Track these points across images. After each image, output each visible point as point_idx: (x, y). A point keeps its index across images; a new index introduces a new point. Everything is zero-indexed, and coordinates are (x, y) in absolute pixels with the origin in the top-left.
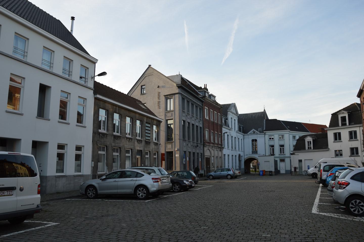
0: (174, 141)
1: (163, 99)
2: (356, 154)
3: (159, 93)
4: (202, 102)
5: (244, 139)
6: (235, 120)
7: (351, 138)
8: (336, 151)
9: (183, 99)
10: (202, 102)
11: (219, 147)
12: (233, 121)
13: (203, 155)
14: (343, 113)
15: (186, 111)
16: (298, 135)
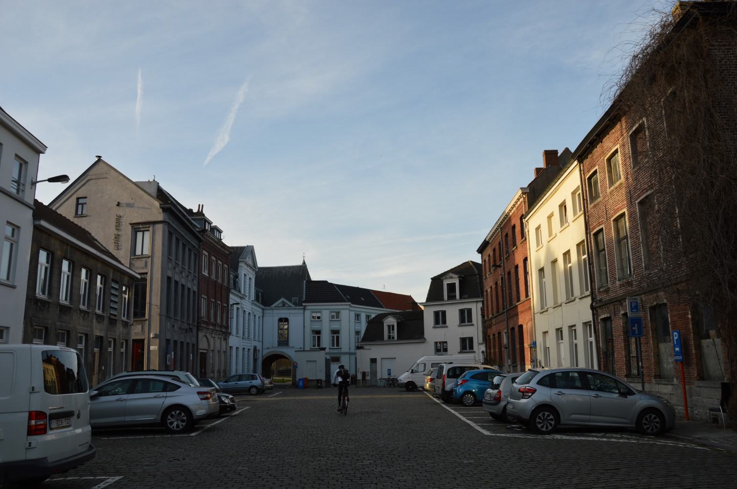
0: (147, 317)
1: (127, 231)
2: (470, 349)
3: (119, 218)
4: (200, 240)
5: (263, 317)
6: (250, 278)
7: (462, 320)
8: (436, 343)
9: (170, 234)
10: (200, 240)
11: (224, 333)
12: (248, 281)
13: (196, 346)
14: (451, 278)
15: (173, 258)
16: (374, 312)
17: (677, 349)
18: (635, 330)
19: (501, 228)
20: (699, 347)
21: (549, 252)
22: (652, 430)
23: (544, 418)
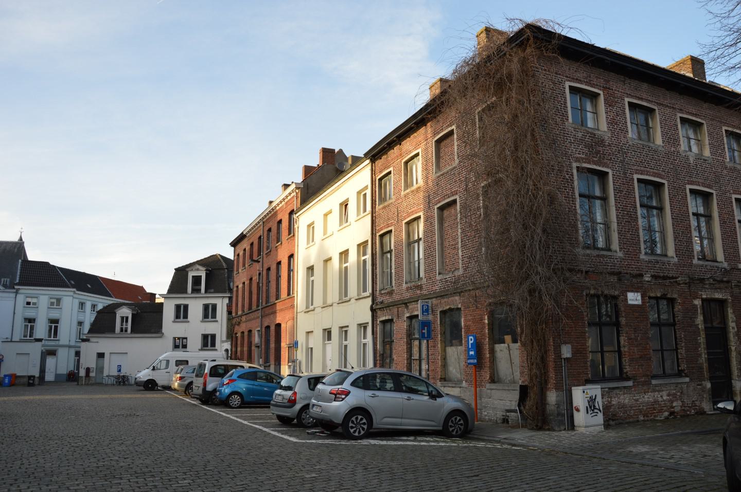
7: (206, 316)
8: (175, 338)
14: (198, 270)
16: (102, 302)
17: (472, 353)
18: (424, 333)
19: (263, 222)
20: (492, 351)
21: (322, 249)
22: (457, 432)
23: (359, 422)
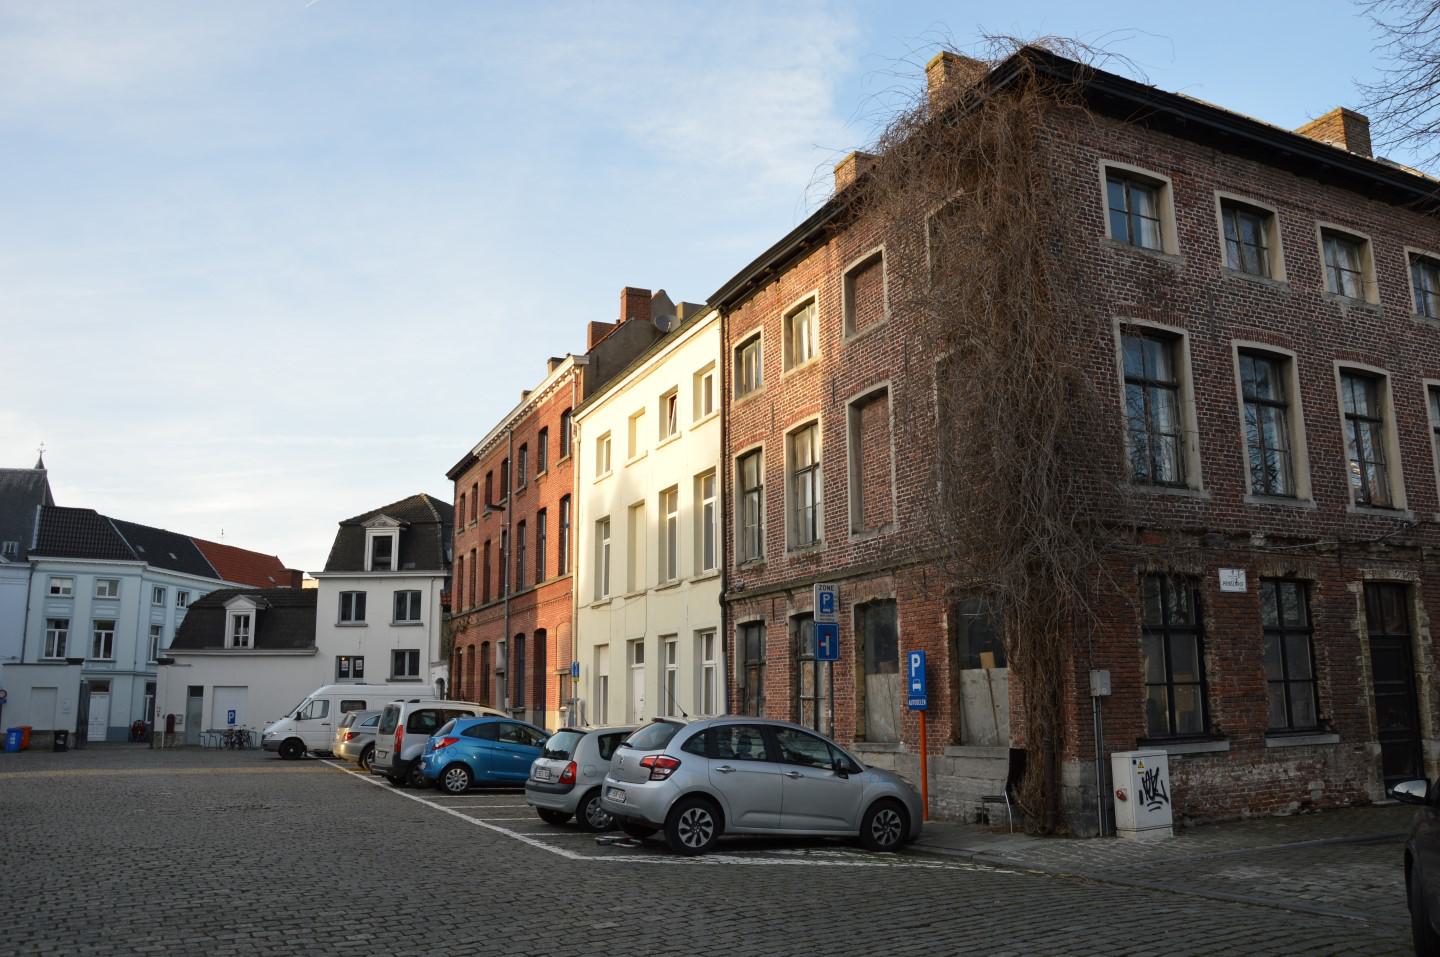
7: (400, 614)
8: (339, 658)
14: (385, 524)
16: (198, 587)
17: (917, 686)
18: (824, 648)
19: (512, 432)
20: (957, 683)
21: (625, 485)
22: (888, 840)
23: (698, 820)
